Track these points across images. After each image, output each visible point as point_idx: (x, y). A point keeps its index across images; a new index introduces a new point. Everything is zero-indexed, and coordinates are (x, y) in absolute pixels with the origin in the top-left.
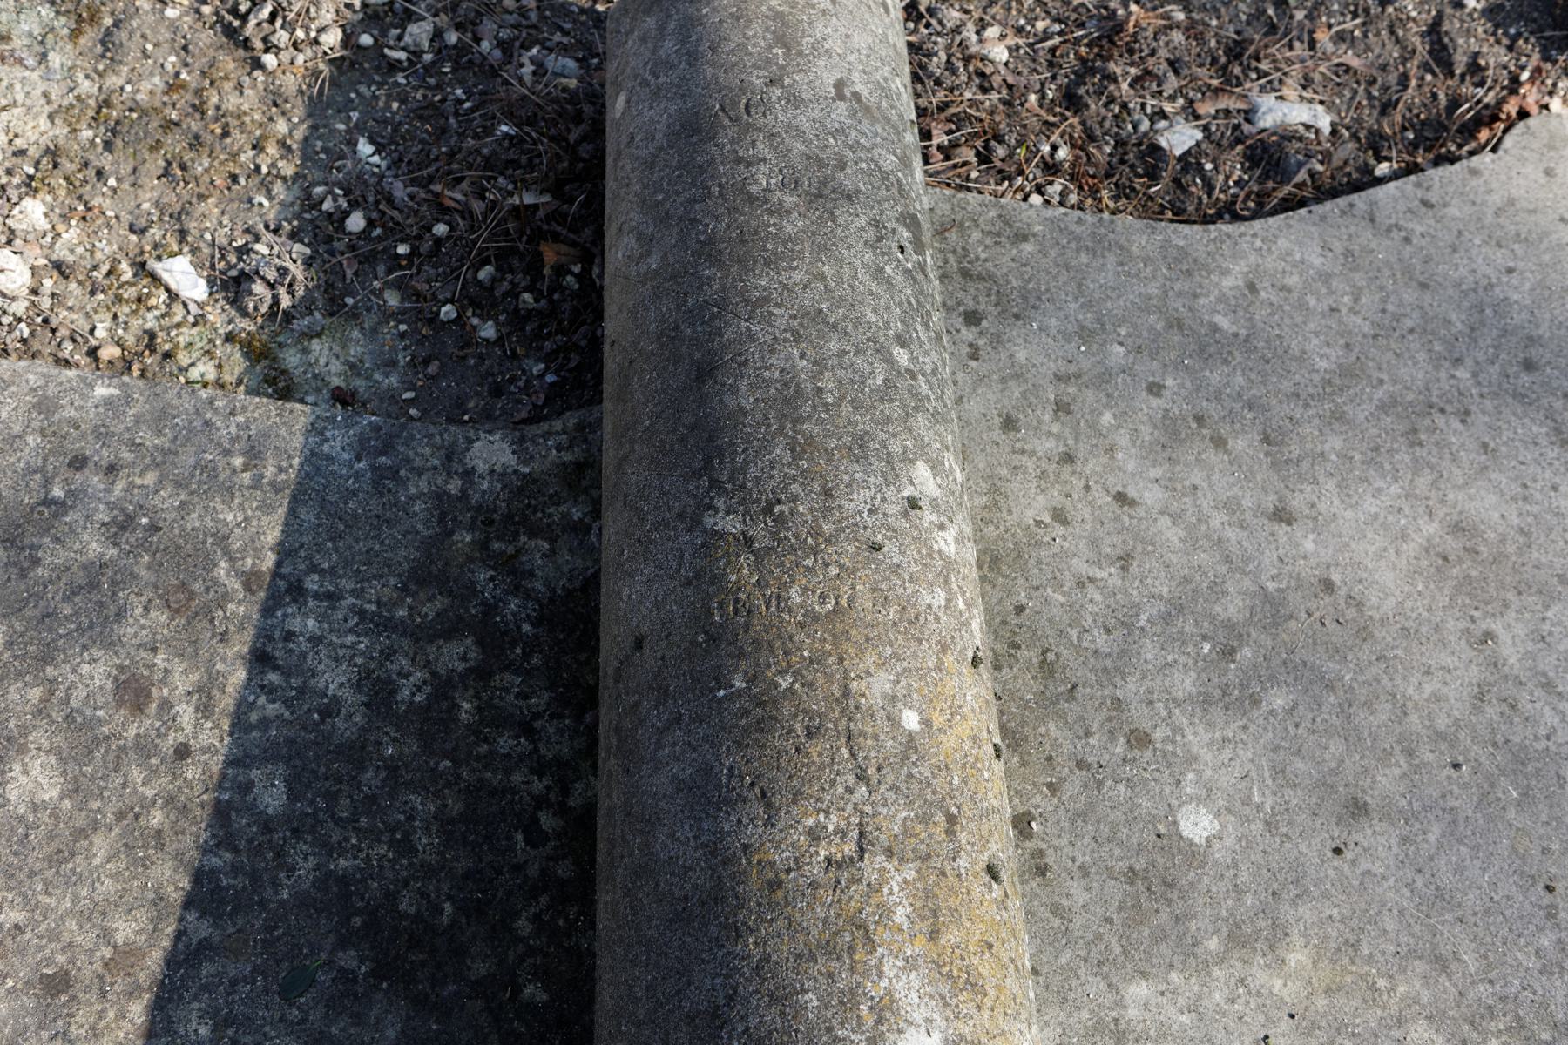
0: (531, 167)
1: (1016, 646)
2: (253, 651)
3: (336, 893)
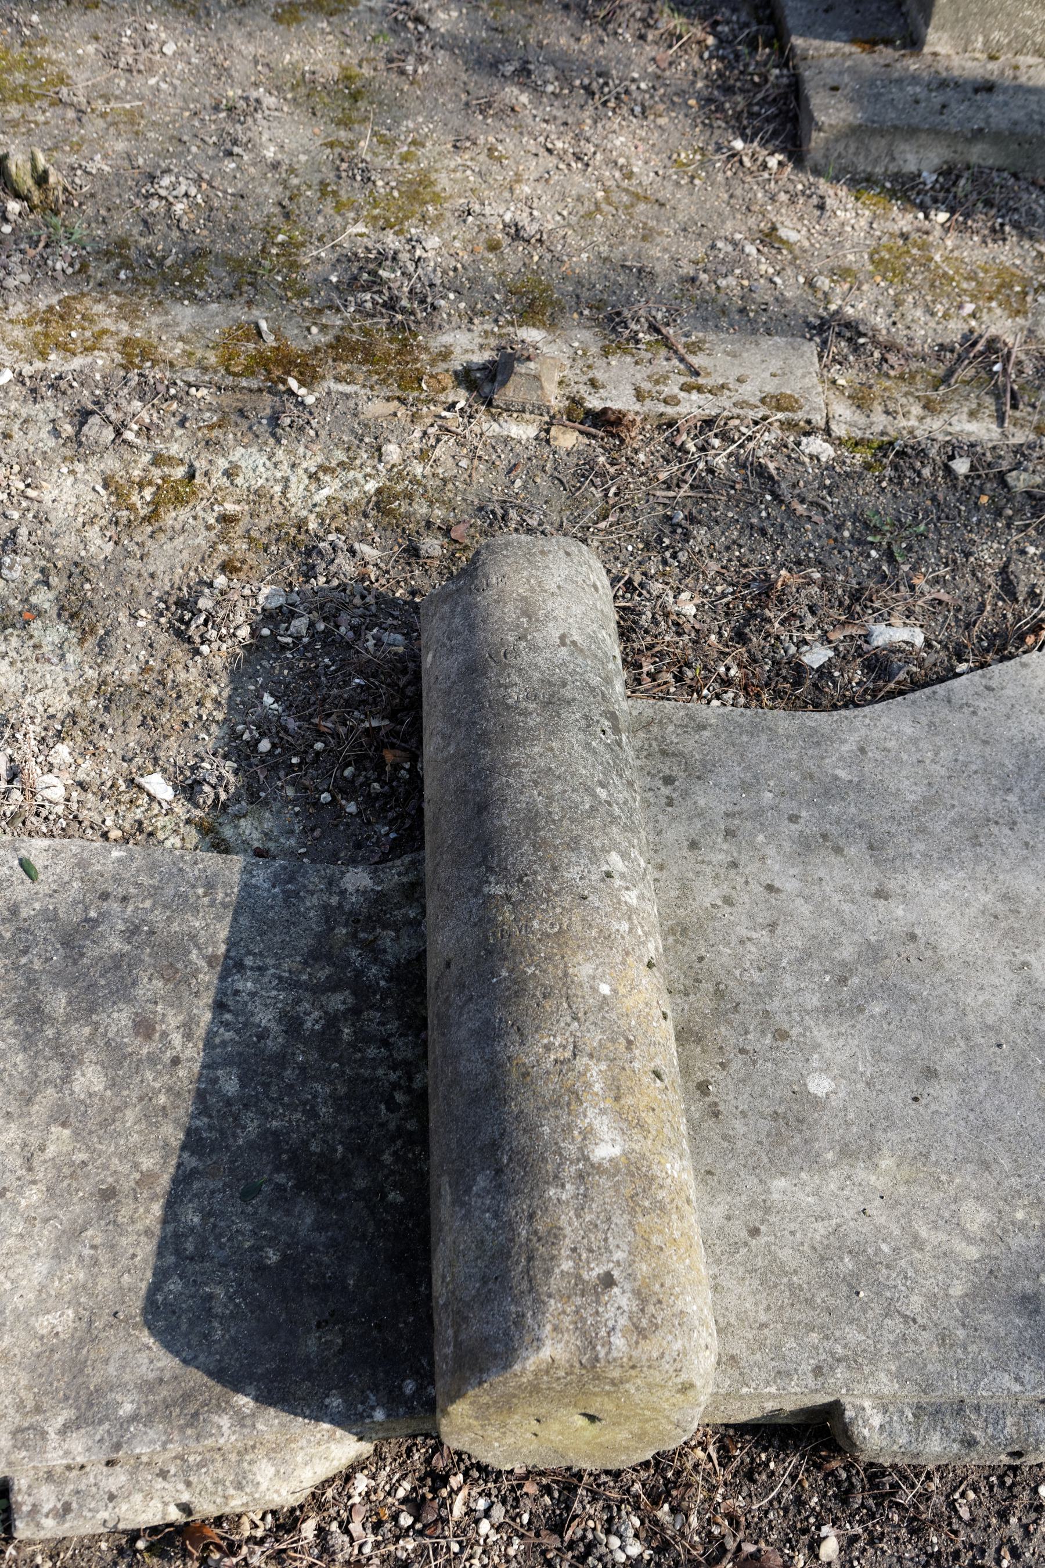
0: (375, 703)
1: (699, 981)
2: (215, 1002)
3: (271, 1141)
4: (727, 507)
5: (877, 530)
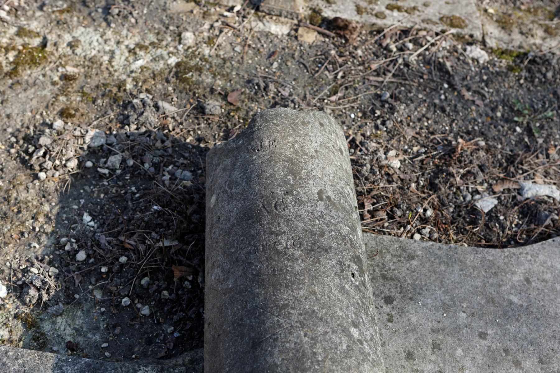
4: (418, 91)
5: (519, 113)
